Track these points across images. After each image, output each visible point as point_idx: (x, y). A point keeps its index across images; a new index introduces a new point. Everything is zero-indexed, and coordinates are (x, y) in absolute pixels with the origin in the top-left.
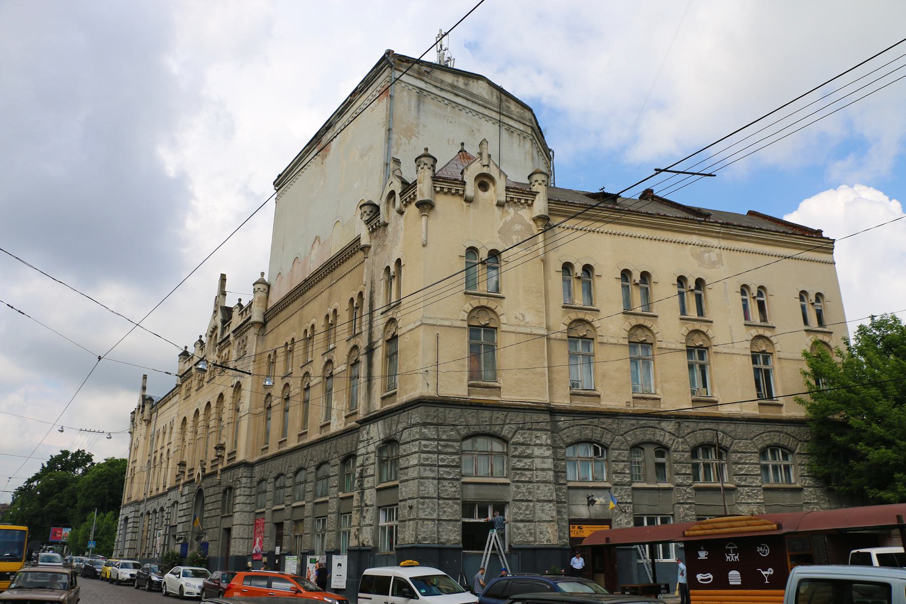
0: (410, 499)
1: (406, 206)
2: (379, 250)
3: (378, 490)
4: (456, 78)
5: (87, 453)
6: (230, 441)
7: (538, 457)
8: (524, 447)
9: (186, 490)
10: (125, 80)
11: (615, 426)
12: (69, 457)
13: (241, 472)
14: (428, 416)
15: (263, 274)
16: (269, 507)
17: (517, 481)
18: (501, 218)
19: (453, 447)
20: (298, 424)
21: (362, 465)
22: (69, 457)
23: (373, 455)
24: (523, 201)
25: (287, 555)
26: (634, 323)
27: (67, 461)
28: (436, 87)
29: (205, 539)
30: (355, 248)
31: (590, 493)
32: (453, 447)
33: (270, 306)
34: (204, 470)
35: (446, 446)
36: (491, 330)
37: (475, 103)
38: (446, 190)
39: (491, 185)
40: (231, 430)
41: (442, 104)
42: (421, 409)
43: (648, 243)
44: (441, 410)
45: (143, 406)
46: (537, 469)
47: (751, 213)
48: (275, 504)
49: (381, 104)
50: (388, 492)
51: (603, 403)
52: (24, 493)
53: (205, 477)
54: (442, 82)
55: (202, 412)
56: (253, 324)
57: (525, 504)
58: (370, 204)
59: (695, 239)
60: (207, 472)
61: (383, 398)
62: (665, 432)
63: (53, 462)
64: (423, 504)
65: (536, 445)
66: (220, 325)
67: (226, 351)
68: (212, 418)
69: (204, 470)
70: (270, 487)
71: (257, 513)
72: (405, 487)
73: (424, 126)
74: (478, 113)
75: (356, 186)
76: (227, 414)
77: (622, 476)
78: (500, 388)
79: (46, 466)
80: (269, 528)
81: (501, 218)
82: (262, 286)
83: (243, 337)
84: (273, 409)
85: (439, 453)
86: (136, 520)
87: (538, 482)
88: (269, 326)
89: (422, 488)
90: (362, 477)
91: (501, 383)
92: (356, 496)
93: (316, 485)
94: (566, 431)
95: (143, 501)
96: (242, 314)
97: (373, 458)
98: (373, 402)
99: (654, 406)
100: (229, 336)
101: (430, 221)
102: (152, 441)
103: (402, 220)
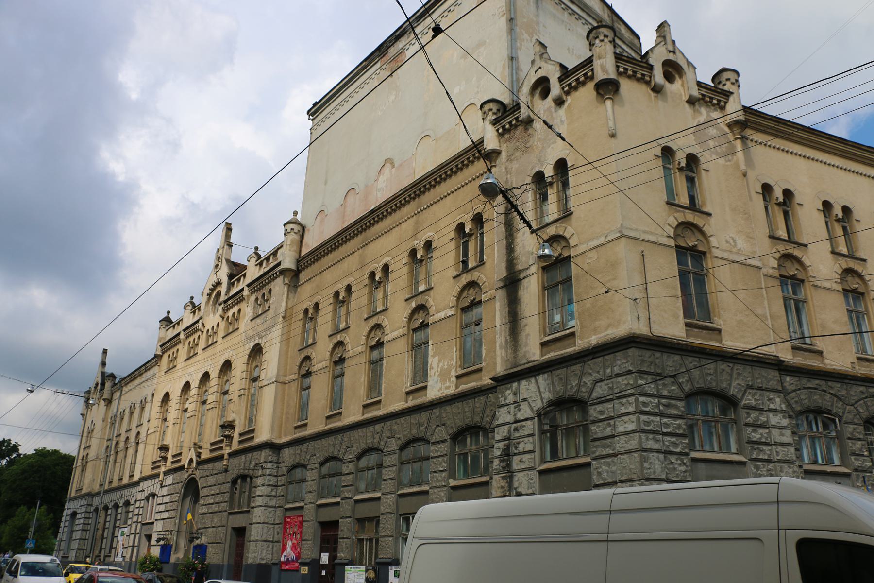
1: (567, 93)
2: (518, 154)
3: (541, 473)
5: (13, 442)
6: (243, 418)
7: (774, 427)
8: (757, 412)
9: (169, 480)
10: (62, 75)
11: (844, 392)
13: (264, 455)
14: (643, 361)
15: (295, 213)
16: (309, 499)
17: (756, 460)
19: (676, 407)
20: (362, 391)
21: (508, 438)
25: (347, 564)
29: (204, 540)
30: (477, 151)
32: (676, 407)
33: (302, 254)
34: (199, 455)
35: (667, 406)
38: (630, 73)
39: (677, 76)
40: (243, 405)
41: (559, 7)
42: (632, 352)
43: (842, 173)
44: (658, 354)
45: (103, 384)
46: (776, 444)
47: (674, 42)
48: (320, 495)
51: (827, 362)
53: (200, 463)
55: (194, 385)
56: (283, 272)
65: (770, 410)
66: (225, 280)
67: (235, 310)
68: (211, 391)
69: (199, 455)
70: (311, 475)
71: (287, 509)
72: (608, 464)
73: (544, 26)
77: (861, 458)
78: (719, 331)
80: (310, 529)
81: (694, 118)
82: (296, 228)
83: (265, 290)
84: (387, 350)
85: (662, 415)
86: (87, 515)
87: (779, 461)
88: (303, 276)
89: (646, 465)
90: (507, 455)
93: (400, 470)
94: (793, 394)
95: (98, 493)
98: (522, 351)
100: (242, 290)
101: (616, 107)
102: (113, 424)
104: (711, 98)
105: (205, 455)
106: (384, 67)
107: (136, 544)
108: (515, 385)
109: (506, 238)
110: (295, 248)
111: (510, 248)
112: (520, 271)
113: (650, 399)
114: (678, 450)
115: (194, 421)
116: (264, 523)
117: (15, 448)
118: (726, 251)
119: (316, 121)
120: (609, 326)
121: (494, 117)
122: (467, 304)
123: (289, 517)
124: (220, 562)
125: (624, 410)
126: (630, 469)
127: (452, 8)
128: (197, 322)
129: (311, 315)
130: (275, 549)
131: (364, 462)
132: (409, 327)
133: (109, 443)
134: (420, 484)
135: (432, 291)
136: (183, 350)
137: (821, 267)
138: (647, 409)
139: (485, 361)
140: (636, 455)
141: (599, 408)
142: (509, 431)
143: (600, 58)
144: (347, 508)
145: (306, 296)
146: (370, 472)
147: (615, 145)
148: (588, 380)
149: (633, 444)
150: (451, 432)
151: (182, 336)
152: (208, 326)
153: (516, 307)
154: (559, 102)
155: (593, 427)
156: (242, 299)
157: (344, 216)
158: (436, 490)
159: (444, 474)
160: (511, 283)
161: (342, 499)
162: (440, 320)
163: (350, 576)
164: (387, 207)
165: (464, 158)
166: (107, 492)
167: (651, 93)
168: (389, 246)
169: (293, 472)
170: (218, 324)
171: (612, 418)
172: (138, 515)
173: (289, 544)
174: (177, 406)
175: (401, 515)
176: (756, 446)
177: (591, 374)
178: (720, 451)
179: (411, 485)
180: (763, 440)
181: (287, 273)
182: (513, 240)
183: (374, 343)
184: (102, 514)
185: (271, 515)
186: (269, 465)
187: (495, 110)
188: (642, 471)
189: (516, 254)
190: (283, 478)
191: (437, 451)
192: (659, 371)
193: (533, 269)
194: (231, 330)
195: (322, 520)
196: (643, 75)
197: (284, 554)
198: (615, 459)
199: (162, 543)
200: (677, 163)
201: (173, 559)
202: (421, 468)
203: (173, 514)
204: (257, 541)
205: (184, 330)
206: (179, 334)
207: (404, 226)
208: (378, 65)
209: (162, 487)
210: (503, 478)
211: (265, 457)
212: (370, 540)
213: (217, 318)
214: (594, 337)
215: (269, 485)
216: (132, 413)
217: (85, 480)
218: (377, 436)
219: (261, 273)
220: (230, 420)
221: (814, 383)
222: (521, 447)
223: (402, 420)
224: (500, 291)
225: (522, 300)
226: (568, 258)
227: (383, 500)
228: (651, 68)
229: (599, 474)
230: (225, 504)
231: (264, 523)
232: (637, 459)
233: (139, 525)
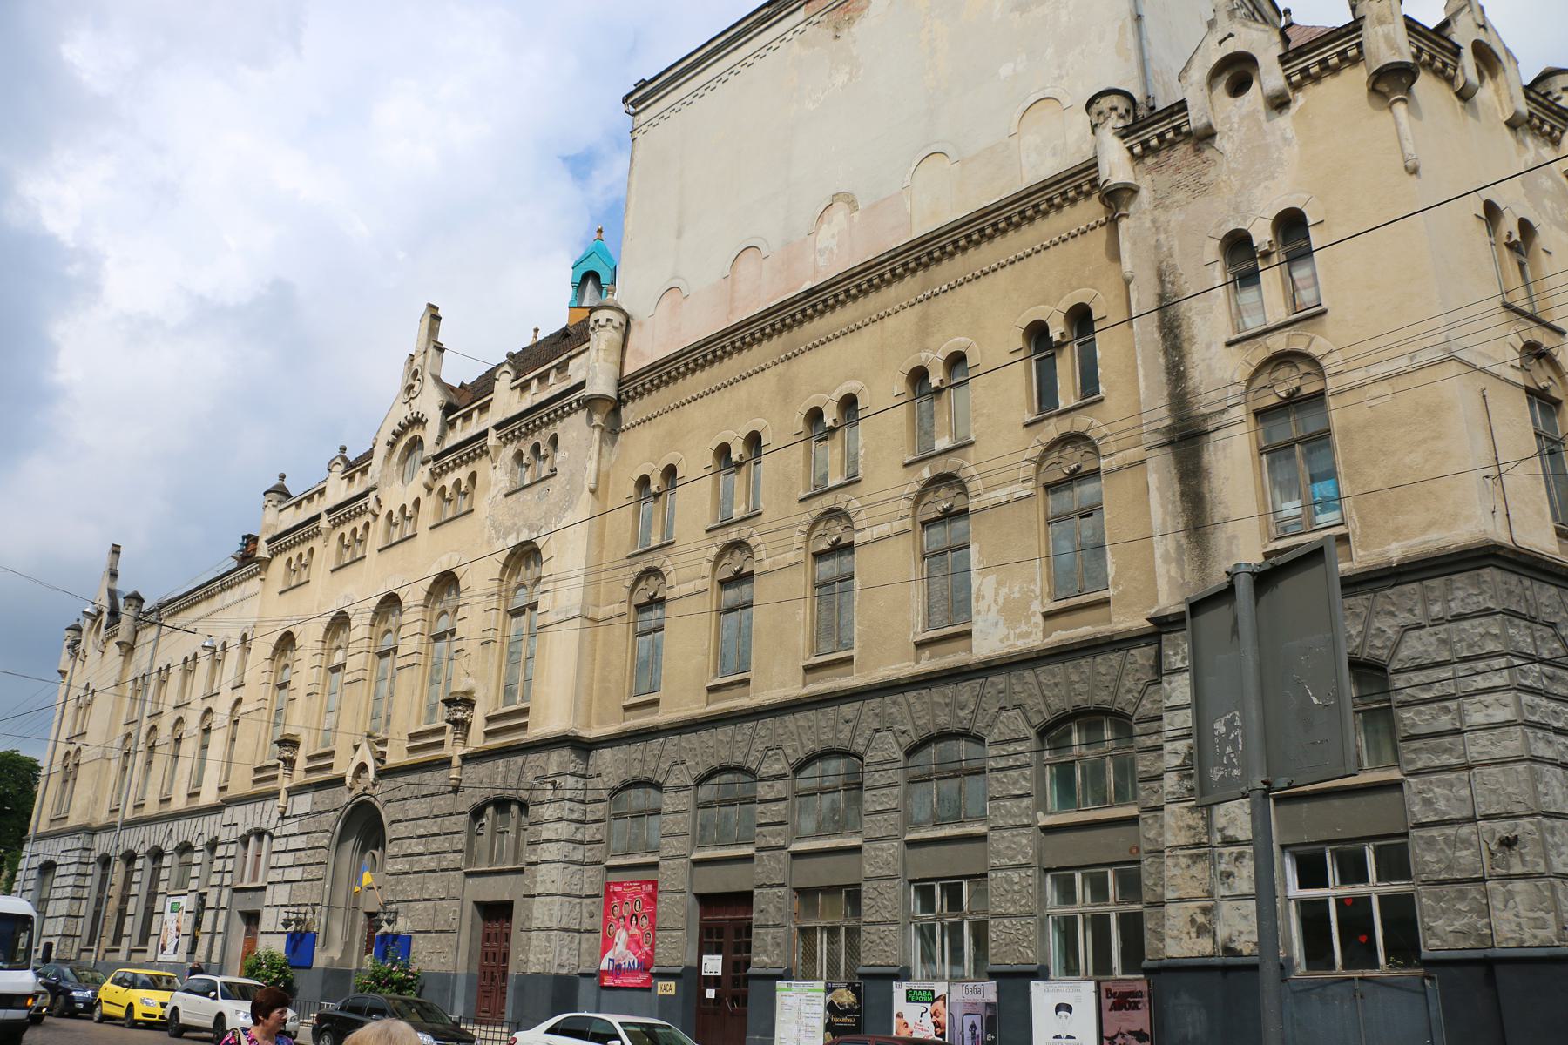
1: (1297, 87)
2: (1180, 196)
9: (303, 803)
13: (555, 761)
25: (781, 978)
30: (1080, 182)
33: (628, 371)
34: (381, 758)
42: (1489, 574)
47: (1482, 8)
50: (1337, 803)
53: (382, 774)
56: (590, 403)
58: (1373, 89)
64: (1552, 831)
66: (434, 416)
67: (462, 473)
69: (381, 758)
71: (611, 869)
83: (542, 437)
86: (82, 869)
88: (629, 413)
105: (397, 755)
106: (815, 19)
107: (220, 928)
109: (1166, 352)
110: (616, 357)
112: (1205, 417)
115: (362, 691)
116: (563, 895)
119: (643, 117)
120: (1431, 525)
121: (1121, 124)
122: (1059, 476)
123: (617, 884)
124: (449, 968)
125: (1480, 682)
126: (1509, 795)
128: (365, 494)
129: (659, 486)
130: (584, 945)
131: (809, 778)
132: (914, 517)
133: (130, 728)
134: (959, 821)
135: (971, 450)
136: (325, 551)
139: (1116, 585)
140: (1521, 767)
143: (1381, 22)
144: (772, 867)
145: (642, 451)
146: (827, 799)
147: (1421, 191)
148: (1389, 626)
149: (1511, 744)
150: (1036, 720)
151: (324, 523)
153: (1199, 485)
154: (1279, 103)
158: (1005, 834)
159: (1025, 802)
160: (1183, 439)
161: (758, 850)
162: (996, 506)
163: (789, 1001)
164: (847, 285)
165: (1040, 199)
166: (128, 825)
167: (1455, 98)
168: (863, 357)
169: (625, 793)
170: (417, 502)
172: (223, 872)
173: (621, 937)
174: (317, 660)
175: (911, 882)
177: (1393, 614)
179: (938, 822)
181: (600, 405)
182: (1182, 357)
183: (823, 546)
184: (119, 867)
185: (575, 880)
186: (571, 781)
187: (1122, 110)
188: (1536, 800)
189: (1191, 384)
190: (600, 806)
192: (1533, 614)
193: (1238, 412)
194: (449, 515)
195: (703, 890)
196: (1445, 65)
197: (609, 955)
200: (1505, 234)
201: (320, 960)
202: (960, 789)
203: (317, 872)
204: (549, 929)
205: (329, 512)
206: (317, 517)
208: (801, 15)
209: (283, 817)
210: (1191, 809)
211: (560, 764)
213: (416, 488)
214: (1394, 545)
215: (571, 820)
218: (847, 729)
220: (461, 689)
223: (911, 696)
224: (1157, 452)
225: (1213, 471)
228: (1456, 51)
230: (459, 856)
231: (563, 895)
232: (1524, 776)
233: (226, 892)
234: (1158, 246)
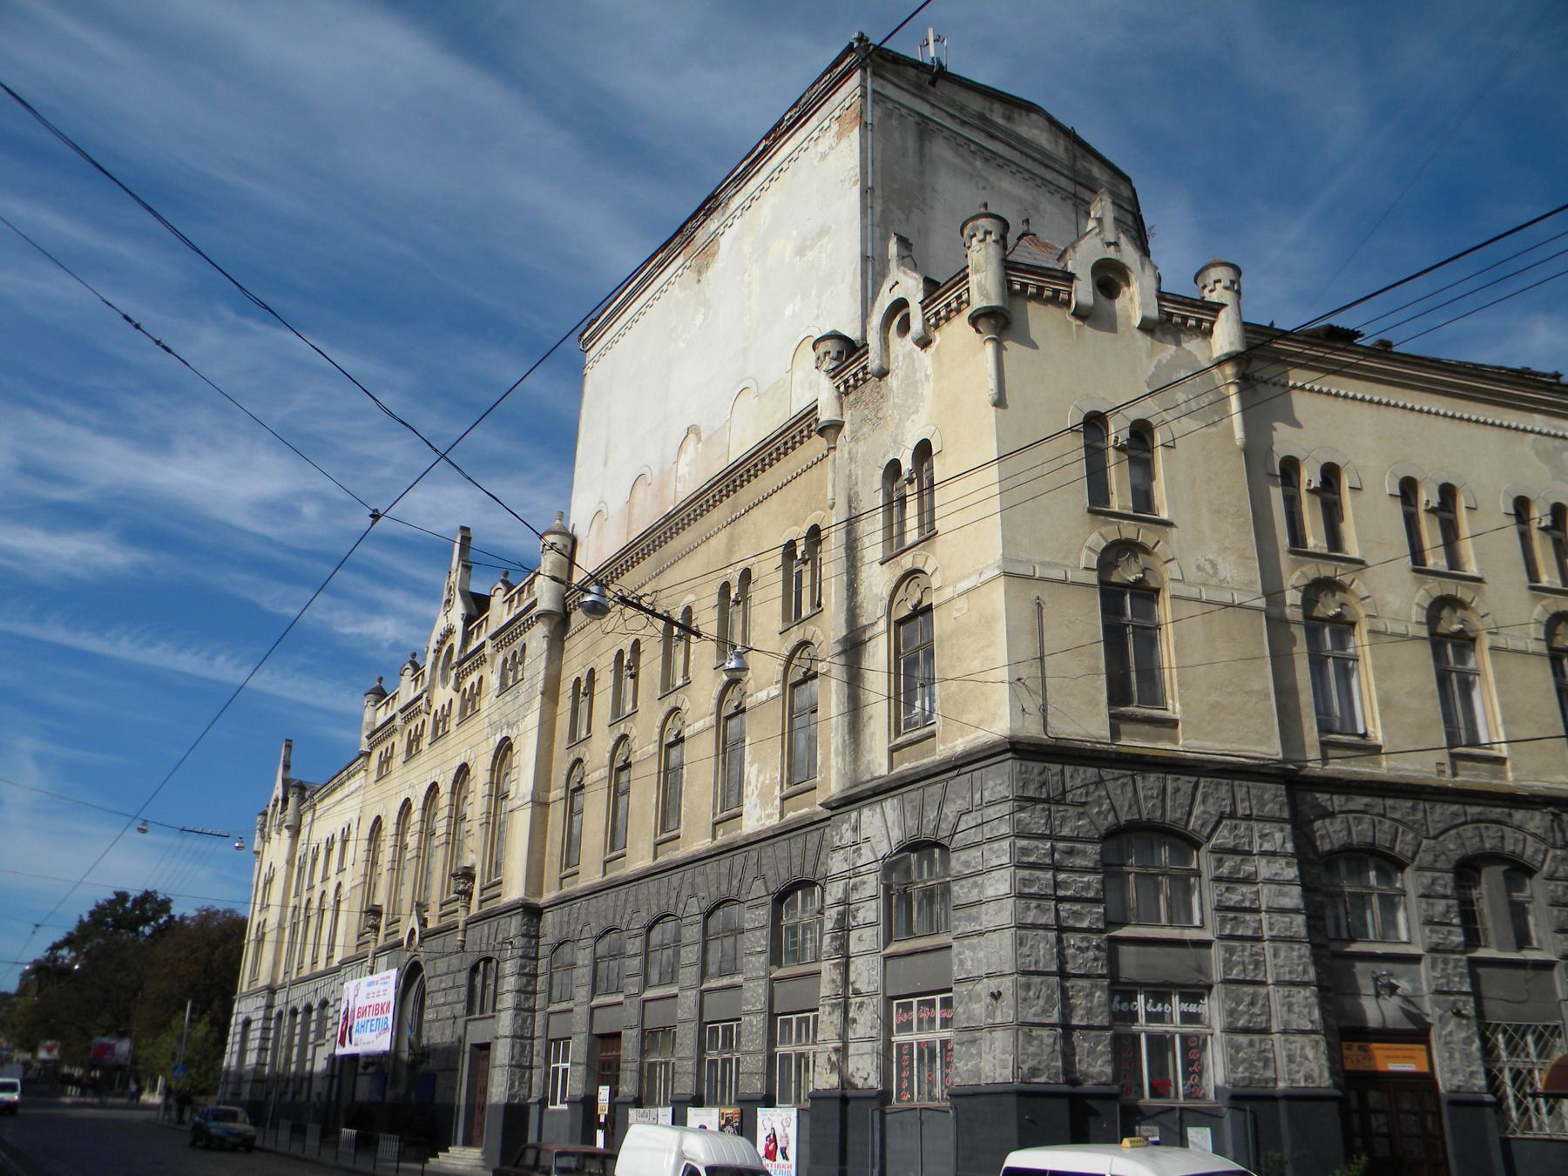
0: (989, 976)
2: (866, 429)
3: (887, 958)
4: (987, 105)
8: (1238, 858)
12: (128, 905)
18: (1151, 355)
22: (128, 905)
23: (872, 877)
24: (1192, 322)
26: (1437, 593)
27: (125, 910)
28: (952, 116)
30: (805, 426)
31: (1383, 968)
34: (423, 923)
36: (1147, 594)
37: (1028, 156)
44: (1056, 768)
49: (845, 142)
52: (45, 972)
54: (962, 108)
57: (1250, 989)
59: (1538, 422)
60: (430, 925)
61: (893, 750)
62: (1526, 834)
63: (99, 914)
65: (1263, 854)
66: (459, 625)
67: (473, 678)
69: (423, 923)
72: (973, 948)
74: (1033, 176)
75: (788, 311)
76: (476, 806)
77: (1445, 929)
79: (86, 918)
81: (1151, 355)
83: (516, 646)
84: (635, 772)
85: (1057, 868)
91: (1174, 707)
92: (828, 970)
96: (511, 600)
97: (871, 884)
98: (866, 758)
99: (1495, 775)
100: (483, 645)
103: (925, 358)
104: (1185, 318)
108: (854, 815)
111: (852, 589)
112: (865, 628)
113: (1034, 843)
114: (1085, 924)
117: (165, 905)
118: (1195, 584)
127: (785, 166)
128: (419, 698)
137: (1390, 597)
138: (1032, 859)
141: (964, 856)
142: (845, 890)
143: (977, 271)
144: (631, 1012)
150: (772, 889)
151: (398, 722)
152: (436, 706)
155: (955, 888)
156: (483, 661)
157: (629, 522)
161: (627, 997)
171: (980, 873)
176: (1231, 915)
178: (1171, 923)
180: (1247, 904)
187: (834, 354)
189: (860, 598)
191: (754, 921)
198: (982, 939)
199: (371, 1070)
205: (402, 711)
207: (713, 541)
208: (680, 260)
212: (667, 1064)
216: (329, 851)
217: (260, 966)
219: (511, 616)
221: (1359, 802)
222: (861, 916)
226: (929, 608)
227: (680, 1000)
229: (961, 963)
234: (850, 476)
